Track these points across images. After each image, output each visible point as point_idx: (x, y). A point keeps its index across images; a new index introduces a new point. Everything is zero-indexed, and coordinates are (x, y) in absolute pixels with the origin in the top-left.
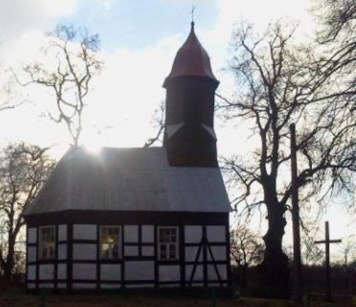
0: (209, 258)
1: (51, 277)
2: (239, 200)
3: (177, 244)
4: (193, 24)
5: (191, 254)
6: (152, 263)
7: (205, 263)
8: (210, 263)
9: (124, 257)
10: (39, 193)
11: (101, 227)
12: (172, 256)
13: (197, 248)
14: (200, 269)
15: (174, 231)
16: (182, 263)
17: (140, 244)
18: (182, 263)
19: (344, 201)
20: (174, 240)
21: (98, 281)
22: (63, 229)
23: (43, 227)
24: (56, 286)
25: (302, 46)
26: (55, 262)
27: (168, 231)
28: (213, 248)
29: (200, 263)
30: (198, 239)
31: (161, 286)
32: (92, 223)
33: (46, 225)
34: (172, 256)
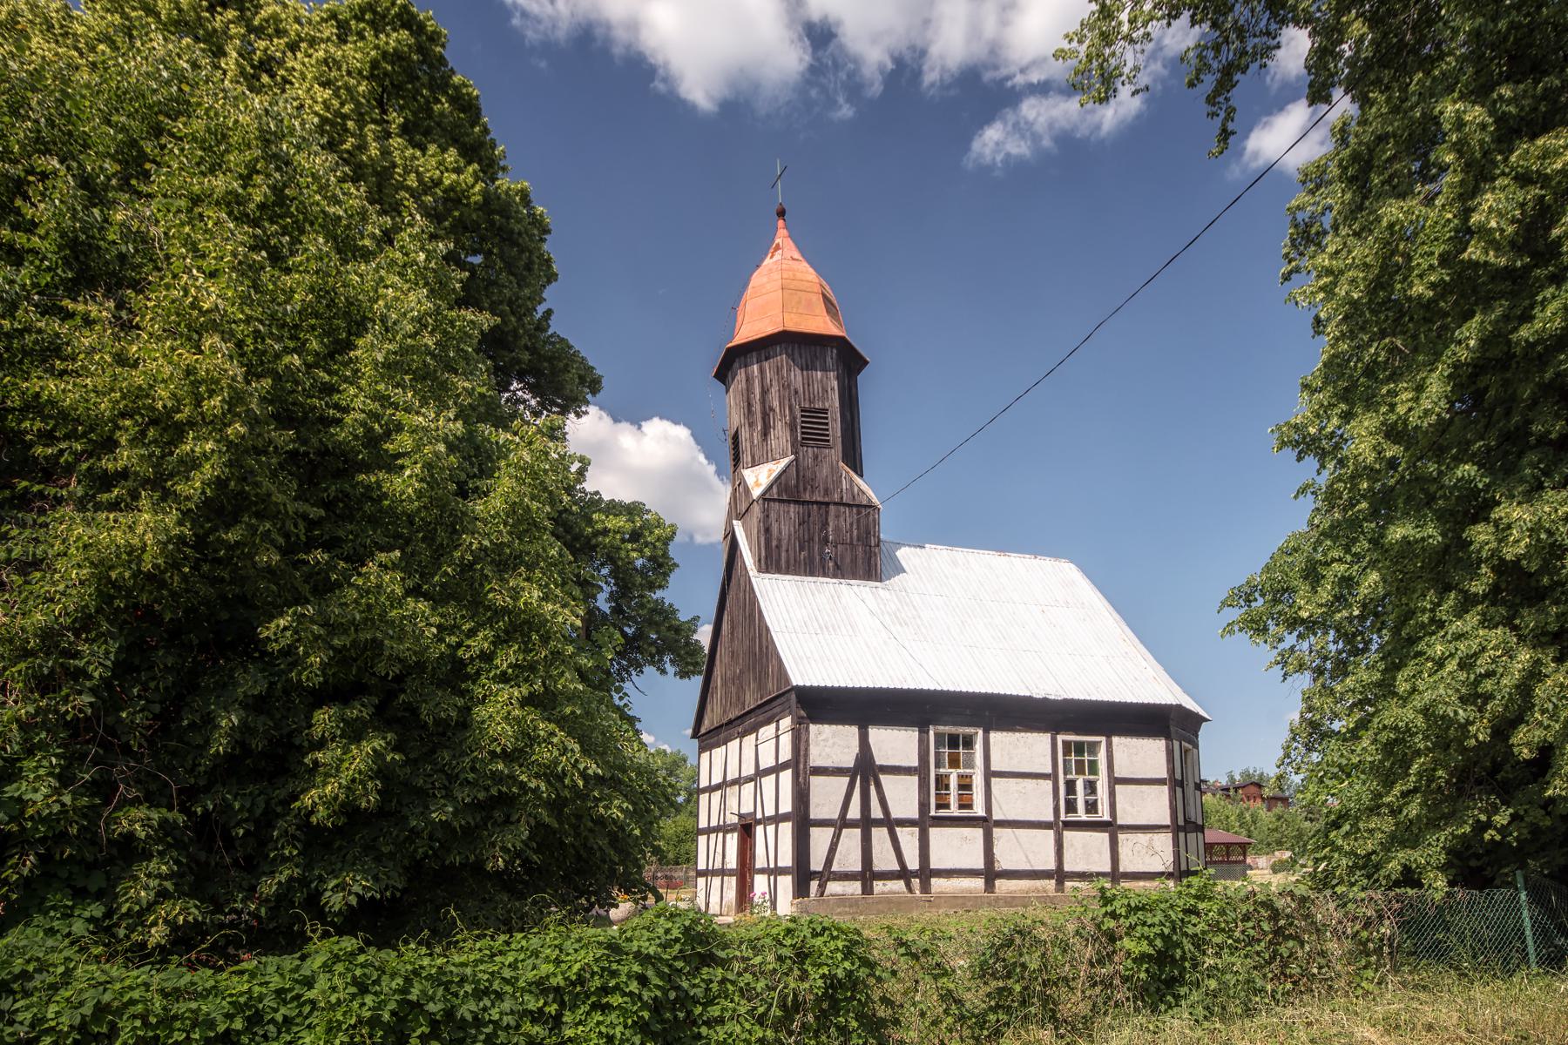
0: (876, 813)
7: (866, 824)
11: (1060, 738)
13: (846, 780)
16: (924, 823)
21: (990, 874)
23: (941, 728)
24: (762, 871)
25: (792, 42)
27: (1080, 749)
28: (883, 778)
29: (852, 824)
30: (848, 759)
32: (851, 724)
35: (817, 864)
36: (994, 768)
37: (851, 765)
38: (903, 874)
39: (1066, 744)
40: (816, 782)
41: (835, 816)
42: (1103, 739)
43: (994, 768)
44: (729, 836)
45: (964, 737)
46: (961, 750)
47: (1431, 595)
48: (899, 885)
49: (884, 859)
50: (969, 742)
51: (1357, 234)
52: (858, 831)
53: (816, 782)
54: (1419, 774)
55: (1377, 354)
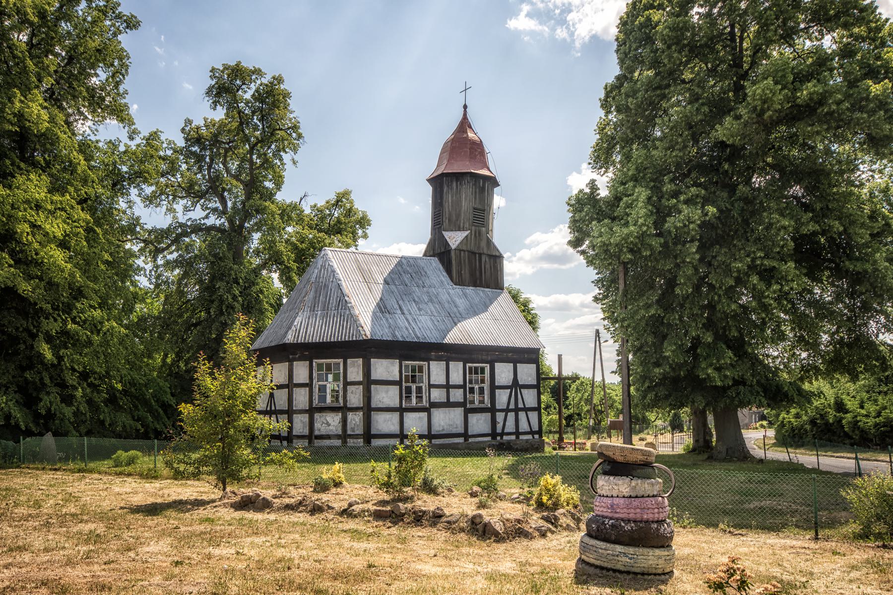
0: (521, 405)
1: (487, 429)
2: (598, 342)
3: (486, 386)
4: (465, 107)
5: (502, 398)
6: (459, 411)
8: (521, 410)
9: (288, 388)
10: (812, 451)
11: (468, 365)
12: (482, 402)
14: (511, 416)
15: (483, 370)
17: (448, 387)
18: (492, 410)
19: (734, 134)
20: (483, 381)
22: (355, 371)
23: (470, 365)
26: (344, 410)
29: (511, 410)
31: (471, 440)
33: (716, 431)
34: (482, 402)
35: (499, 430)
37: (510, 384)
38: (532, 433)
39: (470, 368)
40: (360, 378)
42: (341, 361)
47: (890, 305)
48: (530, 437)
49: (524, 426)
50: (421, 369)
51: (17, 402)
52: (513, 413)
53: (360, 378)
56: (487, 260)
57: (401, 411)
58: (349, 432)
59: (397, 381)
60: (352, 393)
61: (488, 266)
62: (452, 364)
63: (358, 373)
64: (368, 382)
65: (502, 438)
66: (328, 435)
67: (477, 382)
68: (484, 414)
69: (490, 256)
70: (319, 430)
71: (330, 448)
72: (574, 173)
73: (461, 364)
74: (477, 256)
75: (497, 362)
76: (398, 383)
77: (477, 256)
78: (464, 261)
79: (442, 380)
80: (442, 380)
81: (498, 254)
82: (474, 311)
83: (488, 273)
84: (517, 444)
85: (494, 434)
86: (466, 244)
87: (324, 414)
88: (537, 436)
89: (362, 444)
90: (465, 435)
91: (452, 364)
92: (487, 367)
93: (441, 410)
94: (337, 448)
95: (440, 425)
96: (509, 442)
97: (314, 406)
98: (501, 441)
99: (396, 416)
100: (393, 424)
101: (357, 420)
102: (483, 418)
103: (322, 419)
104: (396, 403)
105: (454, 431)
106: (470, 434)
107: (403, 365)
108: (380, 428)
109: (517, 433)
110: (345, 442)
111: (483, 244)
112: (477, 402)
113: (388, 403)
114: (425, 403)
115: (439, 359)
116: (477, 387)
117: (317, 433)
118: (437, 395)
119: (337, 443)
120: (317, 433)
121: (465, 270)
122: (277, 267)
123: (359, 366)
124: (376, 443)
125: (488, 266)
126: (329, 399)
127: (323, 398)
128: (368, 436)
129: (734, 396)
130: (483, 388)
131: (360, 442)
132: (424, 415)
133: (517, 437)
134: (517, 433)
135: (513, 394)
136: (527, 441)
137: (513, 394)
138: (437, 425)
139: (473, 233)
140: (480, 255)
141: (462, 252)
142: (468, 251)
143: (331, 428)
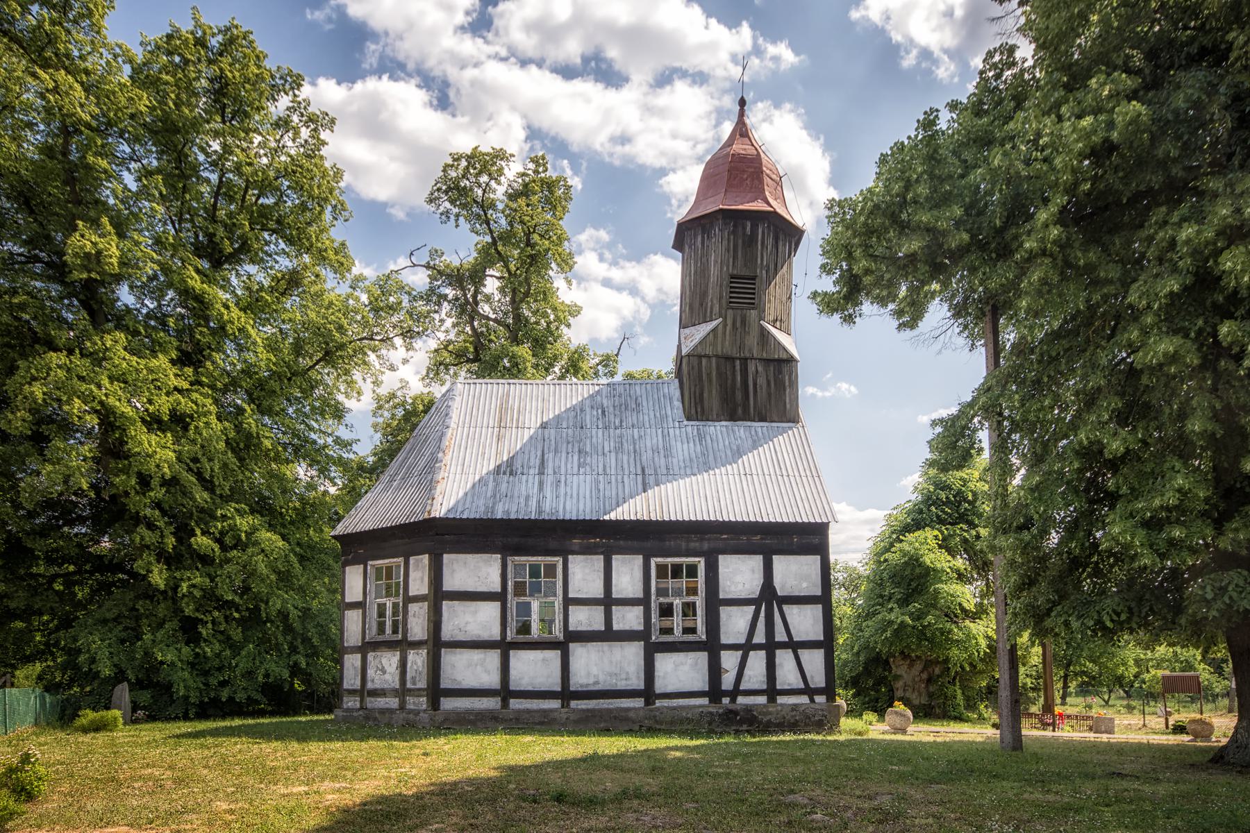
0: (780, 636)
3: (699, 601)
5: (735, 624)
7: (771, 647)
8: (783, 645)
15: (692, 571)
17: (608, 601)
20: (693, 591)
23: (659, 560)
27: (677, 571)
29: (758, 647)
31: (658, 703)
34: (687, 631)
35: (728, 681)
36: (497, 605)
41: (742, 641)
43: (497, 605)
44: (357, 684)
45: (687, 566)
46: (542, 580)
48: (804, 699)
50: (551, 571)
52: (763, 653)
54: (726, 743)
55: (1031, 126)
56: (760, 369)
57: (505, 647)
58: (409, 685)
59: (496, 593)
60: (414, 615)
61: (761, 381)
62: (617, 560)
63: (422, 579)
64: (438, 595)
65: (733, 700)
66: (383, 690)
67: (678, 593)
68: (692, 655)
69: (767, 361)
70: (373, 681)
71: (383, 711)
72: (334, 81)
73: (639, 559)
74: (738, 362)
75: (725, 552)
76: (499, 597)
77: (738, 362)
78: (709, 375)
79: (597, 590)
80: (597, 590)
81: (785, 356)
82: (705, 463)
83: (762, 394)
84: (770, 713)
85: (714, 691)
86: (714, 344)
87: (379, 653)
88: (821, 699)
89: (424, 706)
90: (648, 693)
91: (617, 560)
92: (701, 563)
93: (593, 646)
94: (391, 711)
95: (589, 674)
96: (748, 709)
97: (509, 639)
98: (732, 707)
99: (493, 657)
100: (487, 672)
101: (420, 664)
102: (689, 661)
103: (377, 661)
104: (494, 633)
105: (622, 685)
106: (657, 691)
107: (509, 563)
108: (459, 678)
109: (772, 691)
110: (772, 699)
111: (752, 340)
112: (678, 631)
113: (476, 632)
114: (558, 632)
115: (587, 551)
116: (677, 602)
117: (370, 686)
118: (583, 618)
119: (393, 702)
120: (370, 686)
121: (710, 392)
122: (60, 408)
123: (424, 567)
124: (448, 704)
125: (761, 381)
126: (388, 630)
127: (381, 628)
128: (436, 692)
129: (1209, 596)
130: (694, 604)
131: (423, 702)
132: (554, 656)
133: (505, 704)
134: (772, 691)
135: (762, 614)
136: (795, 707)
137: (762, 614)
138: (583, 673)
139: (729, 322)
140: (744, 361)
141: (704, 361)
142: (717, 356)
143: (387, 677)
